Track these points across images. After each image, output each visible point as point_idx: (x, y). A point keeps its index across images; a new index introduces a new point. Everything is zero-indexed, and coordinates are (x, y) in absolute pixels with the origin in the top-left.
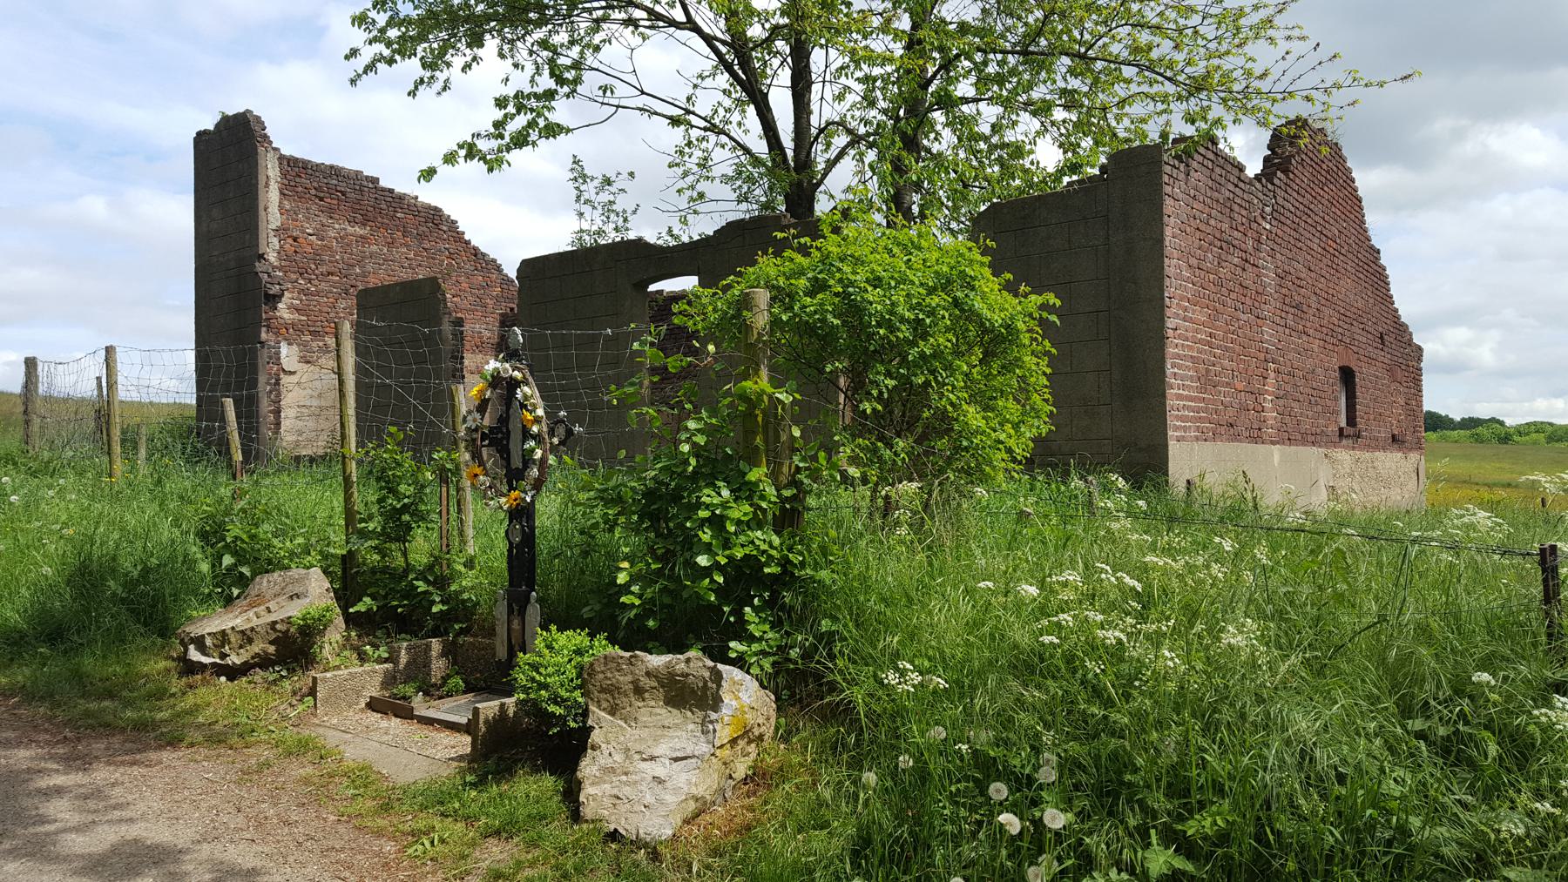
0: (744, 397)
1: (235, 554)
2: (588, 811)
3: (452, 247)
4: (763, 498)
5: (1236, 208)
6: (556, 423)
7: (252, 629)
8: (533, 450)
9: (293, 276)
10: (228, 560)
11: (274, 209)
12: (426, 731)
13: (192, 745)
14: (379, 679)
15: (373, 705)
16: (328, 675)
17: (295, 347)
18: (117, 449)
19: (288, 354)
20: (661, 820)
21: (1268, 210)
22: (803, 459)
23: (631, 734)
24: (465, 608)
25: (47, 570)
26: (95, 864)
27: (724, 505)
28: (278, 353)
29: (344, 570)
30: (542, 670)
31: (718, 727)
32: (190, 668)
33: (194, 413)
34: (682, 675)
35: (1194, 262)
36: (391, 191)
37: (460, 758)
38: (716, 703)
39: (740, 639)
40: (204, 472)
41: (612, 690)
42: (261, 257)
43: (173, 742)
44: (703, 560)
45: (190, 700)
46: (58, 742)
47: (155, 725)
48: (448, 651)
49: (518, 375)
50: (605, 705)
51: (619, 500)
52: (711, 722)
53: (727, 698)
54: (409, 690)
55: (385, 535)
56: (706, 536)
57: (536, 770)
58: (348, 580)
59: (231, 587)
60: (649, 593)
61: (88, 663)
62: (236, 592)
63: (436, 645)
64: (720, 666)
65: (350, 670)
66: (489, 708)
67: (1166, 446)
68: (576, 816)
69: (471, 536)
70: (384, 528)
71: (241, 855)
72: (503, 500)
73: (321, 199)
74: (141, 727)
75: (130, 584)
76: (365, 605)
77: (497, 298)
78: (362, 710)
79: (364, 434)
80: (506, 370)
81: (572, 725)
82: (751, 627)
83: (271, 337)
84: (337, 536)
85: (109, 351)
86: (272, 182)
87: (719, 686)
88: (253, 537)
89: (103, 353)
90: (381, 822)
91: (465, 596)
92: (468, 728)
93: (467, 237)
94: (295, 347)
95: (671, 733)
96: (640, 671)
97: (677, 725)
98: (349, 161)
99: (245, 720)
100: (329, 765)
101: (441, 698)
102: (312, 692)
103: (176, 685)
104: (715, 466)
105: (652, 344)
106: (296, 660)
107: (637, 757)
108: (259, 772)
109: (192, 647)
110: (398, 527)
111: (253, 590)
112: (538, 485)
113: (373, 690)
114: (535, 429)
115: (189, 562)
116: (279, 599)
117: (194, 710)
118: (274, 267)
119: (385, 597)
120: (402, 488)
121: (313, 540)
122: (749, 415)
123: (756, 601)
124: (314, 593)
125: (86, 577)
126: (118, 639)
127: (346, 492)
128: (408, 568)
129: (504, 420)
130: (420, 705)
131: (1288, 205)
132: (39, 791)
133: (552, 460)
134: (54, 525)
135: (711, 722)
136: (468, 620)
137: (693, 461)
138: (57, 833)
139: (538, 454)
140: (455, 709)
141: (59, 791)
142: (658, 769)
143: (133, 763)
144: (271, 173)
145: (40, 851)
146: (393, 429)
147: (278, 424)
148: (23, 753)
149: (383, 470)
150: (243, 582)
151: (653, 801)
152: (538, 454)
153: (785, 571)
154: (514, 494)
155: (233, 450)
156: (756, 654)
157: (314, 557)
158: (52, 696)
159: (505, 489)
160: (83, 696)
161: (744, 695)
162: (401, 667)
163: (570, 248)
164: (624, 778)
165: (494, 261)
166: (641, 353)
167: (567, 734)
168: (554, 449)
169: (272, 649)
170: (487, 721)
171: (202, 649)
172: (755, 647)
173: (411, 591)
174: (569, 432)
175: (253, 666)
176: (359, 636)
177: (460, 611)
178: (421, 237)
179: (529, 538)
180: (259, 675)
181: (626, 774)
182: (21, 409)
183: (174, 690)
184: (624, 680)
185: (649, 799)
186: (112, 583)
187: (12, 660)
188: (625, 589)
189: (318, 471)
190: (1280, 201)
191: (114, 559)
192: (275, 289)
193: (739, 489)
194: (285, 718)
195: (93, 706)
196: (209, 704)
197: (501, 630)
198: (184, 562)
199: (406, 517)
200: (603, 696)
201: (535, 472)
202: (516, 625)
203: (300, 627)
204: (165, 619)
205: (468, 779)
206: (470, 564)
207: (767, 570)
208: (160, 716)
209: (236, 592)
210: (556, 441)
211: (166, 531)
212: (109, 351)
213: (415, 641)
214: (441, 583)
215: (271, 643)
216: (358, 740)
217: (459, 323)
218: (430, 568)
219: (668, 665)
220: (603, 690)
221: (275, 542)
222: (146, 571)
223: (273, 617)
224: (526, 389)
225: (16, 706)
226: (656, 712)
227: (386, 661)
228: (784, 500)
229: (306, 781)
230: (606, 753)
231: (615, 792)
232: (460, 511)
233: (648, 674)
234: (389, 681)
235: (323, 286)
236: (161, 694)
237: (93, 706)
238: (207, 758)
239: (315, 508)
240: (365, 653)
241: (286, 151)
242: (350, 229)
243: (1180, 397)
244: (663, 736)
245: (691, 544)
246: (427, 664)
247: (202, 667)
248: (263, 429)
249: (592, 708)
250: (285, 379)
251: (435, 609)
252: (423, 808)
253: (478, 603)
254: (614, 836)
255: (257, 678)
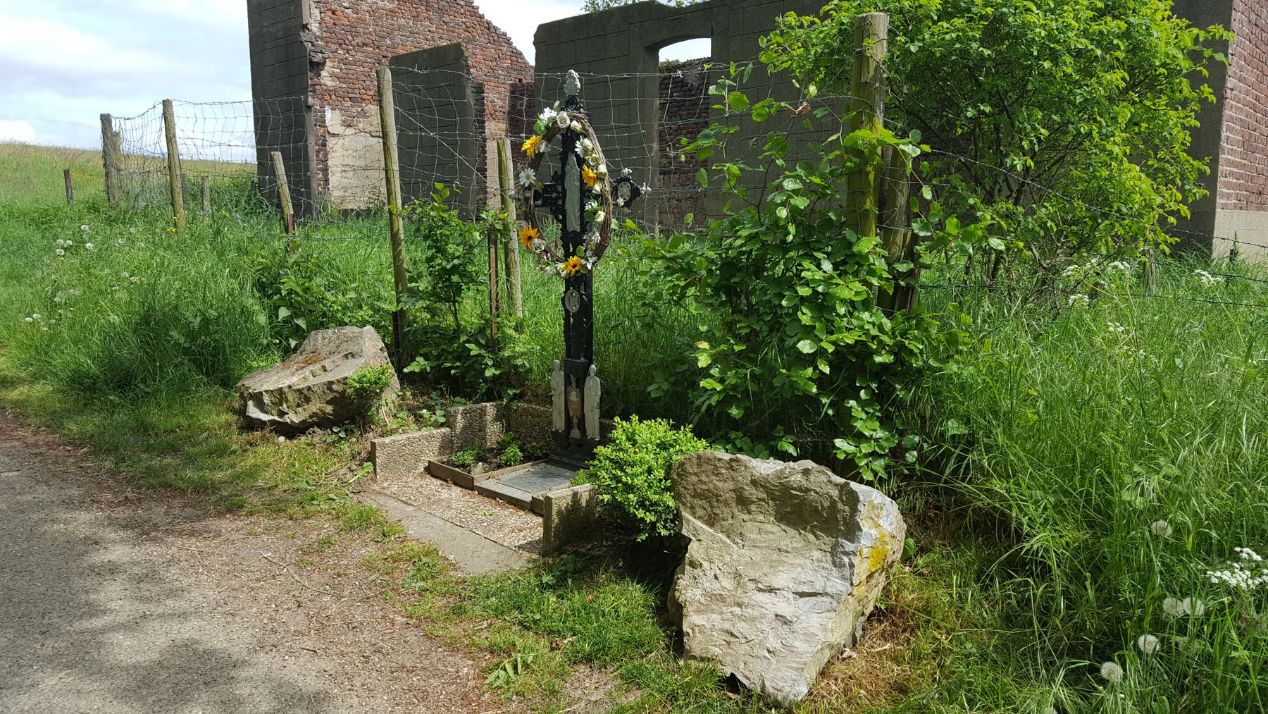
0: (856, 151)
1: (290, 305)
2: (695, 644)
3: (468, 21)
4: (872, 272)
6: (619, 182)
7: (309, 388)
8: (595, 212)
9: (334, 47)
10: (284, 313)
12: (487, 508)
13: (251, 514)
14: (436, 444)
15: (431, 470)
16: (387, 440)
17: (337, 112)
18: (180, 200)
19: (332, 118)
20: (794, 675)
22: (925, 227)
23: (738, 554)
24: (518, 374)
25: (113, 318)
26: (142, 682)
27: (828, 281)
28: (323, 117)
29: (396, 327)
30: (629, 470)
31: (856, 561)
32: (251, 425)
33: (255, 170)
34: (800, 489)
35: (1253, 17)
37: (530, 547)
38: (852, 530)
39: (843, 436)
40: (259, 223)
41: (709, 497)
42: (305, 27)
43: (233, 508)
44: (805, 347)
45: (250, 460)
46: (119, 504)
47: (215, 487)
48: (504, 415)
49: (576, 125)
50: (700, 512)
51: (688, 271)
52: (847, 554)
53: (866, 526)
54: (468, 457)
55: (433, 294)
56: (806, 317)
57: (621, 576)
58: (401, 342)
59: (288, 341)
60: (732, 378)
61: (155, 416)
62: (293, 343)
63: (490, 408)
64: (854, 485)
65: (409, 436)
66: (562, 491)
67: (1214, 213)
68: (678, 644)
69: (525, 300)
70: (434, 288)
71: (304, 672)
72: (561, 266)
74: (202, 488)
75: (191, 335)
76: (416, 366)
77: (507, 69)
78: (421, 475)
79: (409, 191)
80: (563, 120)
81: (664, 532)
82: (859, 425)
83: (317, 101)
84: (388, 292)
85: (166, 104)
87: (854, 510)
88: (306, 290)
89: (161, 107)
90: (454, 631)
91: (519, 362)
92: (538, 507)
93: (481, 12)
94: (337, 112)
95: (791, 559)
96: (743, 479)
97: (797, 550)
99: (304, 485)
100: (393, 548)
101: (499, 467)
102: (371, 457)
103: (237, 440)
104: (815, 232)
105: (731, 89)
106: (353, 421)
107: (751, 585)
108: (320, 551)
109: (250, 403)
110: (448, 286)
111: (308, 345)
112: (599, 251)
113: (432, 456)
114: (597, 188)
115: (246, 314)
116: (335, 358)
117: (253, 473)
118: (316, 37)
119: (438, 357)
120: (451, 248)
121: (365, 295)
122: (859, 172)
123: (862, 393)
124: (362, 355)
125: (151, 325)
126: (182, 388)
127: (394, 250)
128: (458, 330)
129: (560, 178)
130: (479, 474)
132: (92, 568)
133: (614, 224)
134: (134, 269)
135: (847, 554)
136: (522, 385)
137: (792, 229)
138: (104, 631)
139: (601, 216)
140: (517, 480)
141: (112, 569)
142: (784, 605)
143: (192, 534)
145: (83, 658)
146: (439, 186)
147: (326, 181)
148: (84, 516)
149: (431, 229)
150: (300, 334)
151: (779, 646)
152: (601, 216)
153: (899, 361)
154: (573, 260)
155: (284, 203)
156: (866, 456)
157: (365, 313)
158: (117, 449)
159: (560, 253)
160: (147, 450)
161: (882, 520)
162: (458, 431)
163: (583, 12)
164: (737, 610)
165: (505, 34)
166: (720, 99)
167: (656, 540)
168: (618, 213)
169: (329, 409)
170: (559, 512)
171: (261, 406)
172: (865, 448)
173: (463, 354)
174: (635, 192)
175: (311, 425)
176: (414, 395)
177: (512, 377)
179: (586, 308)
180: (319, 435)
181: (739, 605)
182: (102, 162)
183: (234, 447)
184: (725, 487)
185: (773, 643)
186: (174, 333)
187: (85, 405)
188: (705, 373)
189: (364, 224)
191: (176, 307)
192: (318, 58)
193: (844, 262)
194: (345, 483)
195: (156, 462)
196: (268, 465)
197: (559, 401)
198: (242, 312)
199: (455, 278)
200: (697, 502)
201: (597, 237)
202: (574, 396)
203: (356, 390)
204: (227, 370)
205: (546, 579)
206: (519, 328)
207: (878, 359)
208: (219, 475)
209: (293, 343)
210: (621, 202)
211: (225, 284)
212: (166, 104)
213: (470, 406)
214: (493, 346)
215: (328, 403)
216: (421, 514)
217: (479, 89)
218: (481, 331)
220: (696, 495)
221: (328, 295)
222: (206, 321)
223: (330, 377)
224: (587, 141)
225: (85, 457)
226: (766, 530)
227: (442, 425)
228: (897, 276)
229: (369, 566)
230: (710, 574)
231: (727, 626)
232: (508, 274)
233: (754, 483)
234: (447, 445)
235: (359, 56)
236: (221, 451)
237: (156, 462)
238: (267, 530)
239: (364, 264)
240: (421, 416)
243: (1229, 163)
244: (781, 562)
245: (780, 323)
246: (482, 429)
247: (261, 425)
248: (314, 185)
249: (686, 514)
250: (331, 142)
251: (488, 373)
252: (498, 613)
253: (530, 370)
254: (732, 683)
255: (316, 439)
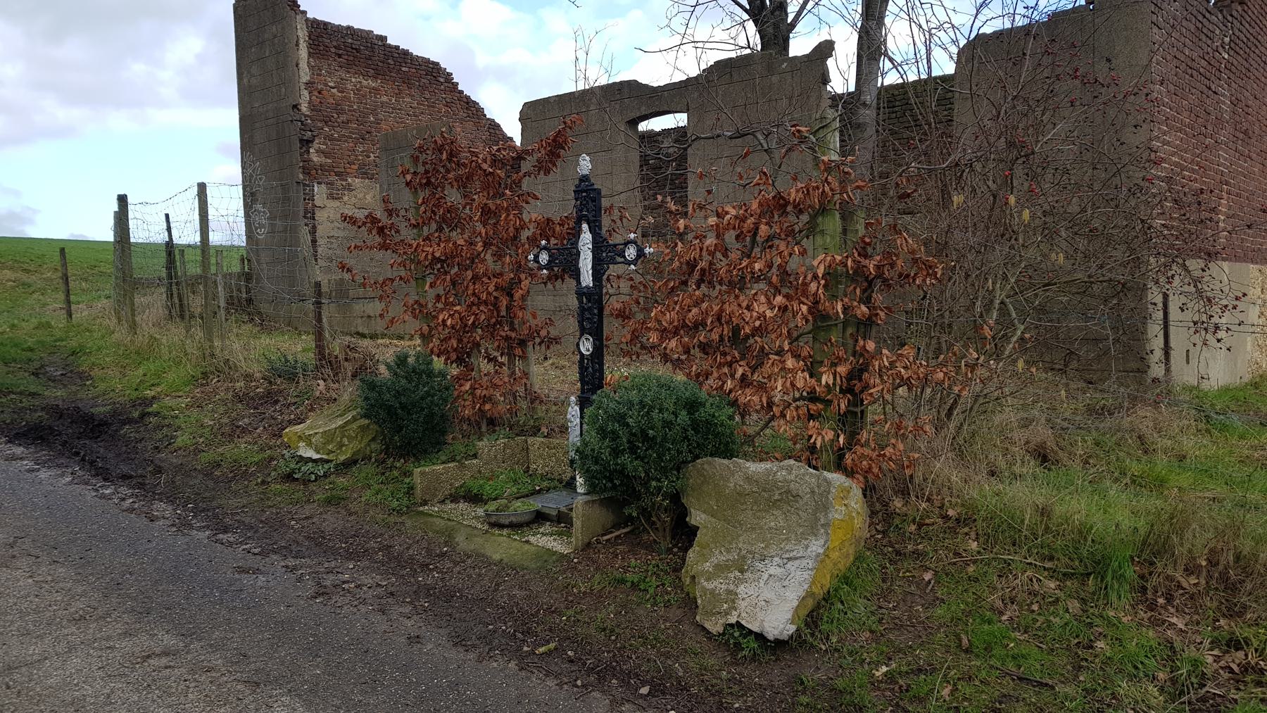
5: (1204, 38)
9: (319, 124)
11: (304, 65)
21: (1227, 40)
36: (397, 48)
73: (340, 56)
85: (202, 188)
86: (301, 41)
89: (195, 189)
98: (357, 25)
131: (1242, 36)
144: (300, 34)
178: (423, 88)
190: (1237, 33)
212: (202, 188)
219: (768, 472)
241: (310, 15)
242: (365, 83)
